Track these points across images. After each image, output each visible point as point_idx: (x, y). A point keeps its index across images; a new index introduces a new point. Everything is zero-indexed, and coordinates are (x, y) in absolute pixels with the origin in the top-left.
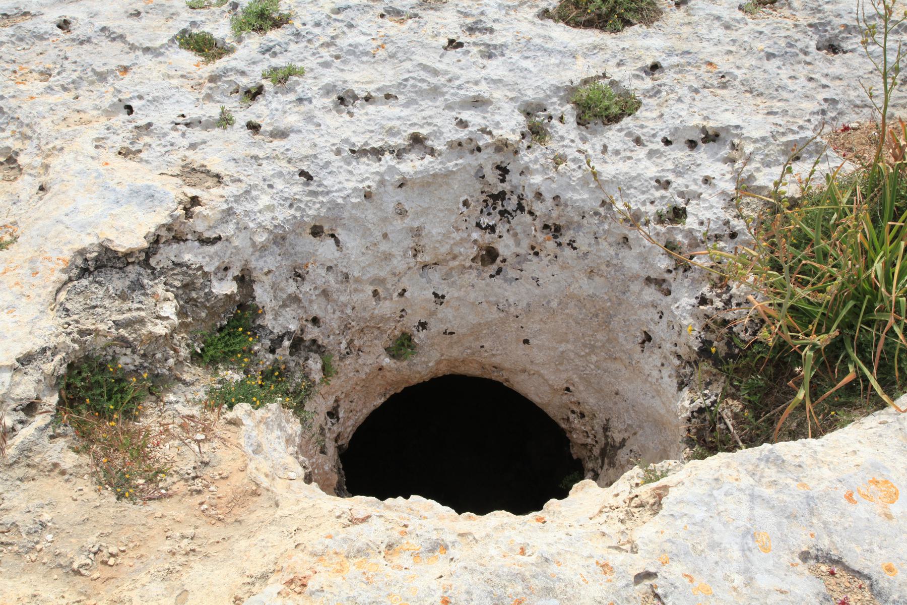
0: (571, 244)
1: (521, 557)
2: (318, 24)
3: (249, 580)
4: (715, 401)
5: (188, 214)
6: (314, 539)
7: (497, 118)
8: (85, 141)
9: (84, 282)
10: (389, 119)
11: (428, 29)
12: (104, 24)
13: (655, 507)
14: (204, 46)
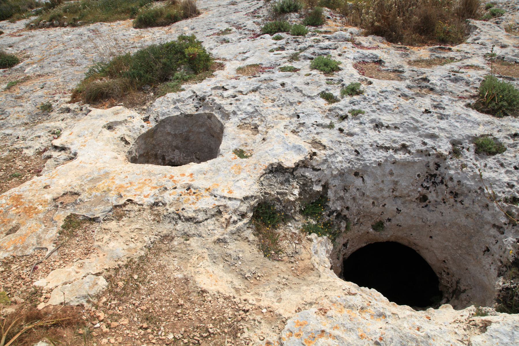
0: (461, 202)
1: (417, 331)
2: (373, 96)
3: (305, 303)
4: (516, 287)
5: (311, 158)
6: (333, 295)
7: (440, 144)
8: (281, 126)
9: (270, 175)
10: (395, 136)
11: (418, 104)
12: (296, 86)
13: (482, 328)
14: (329, 98)
